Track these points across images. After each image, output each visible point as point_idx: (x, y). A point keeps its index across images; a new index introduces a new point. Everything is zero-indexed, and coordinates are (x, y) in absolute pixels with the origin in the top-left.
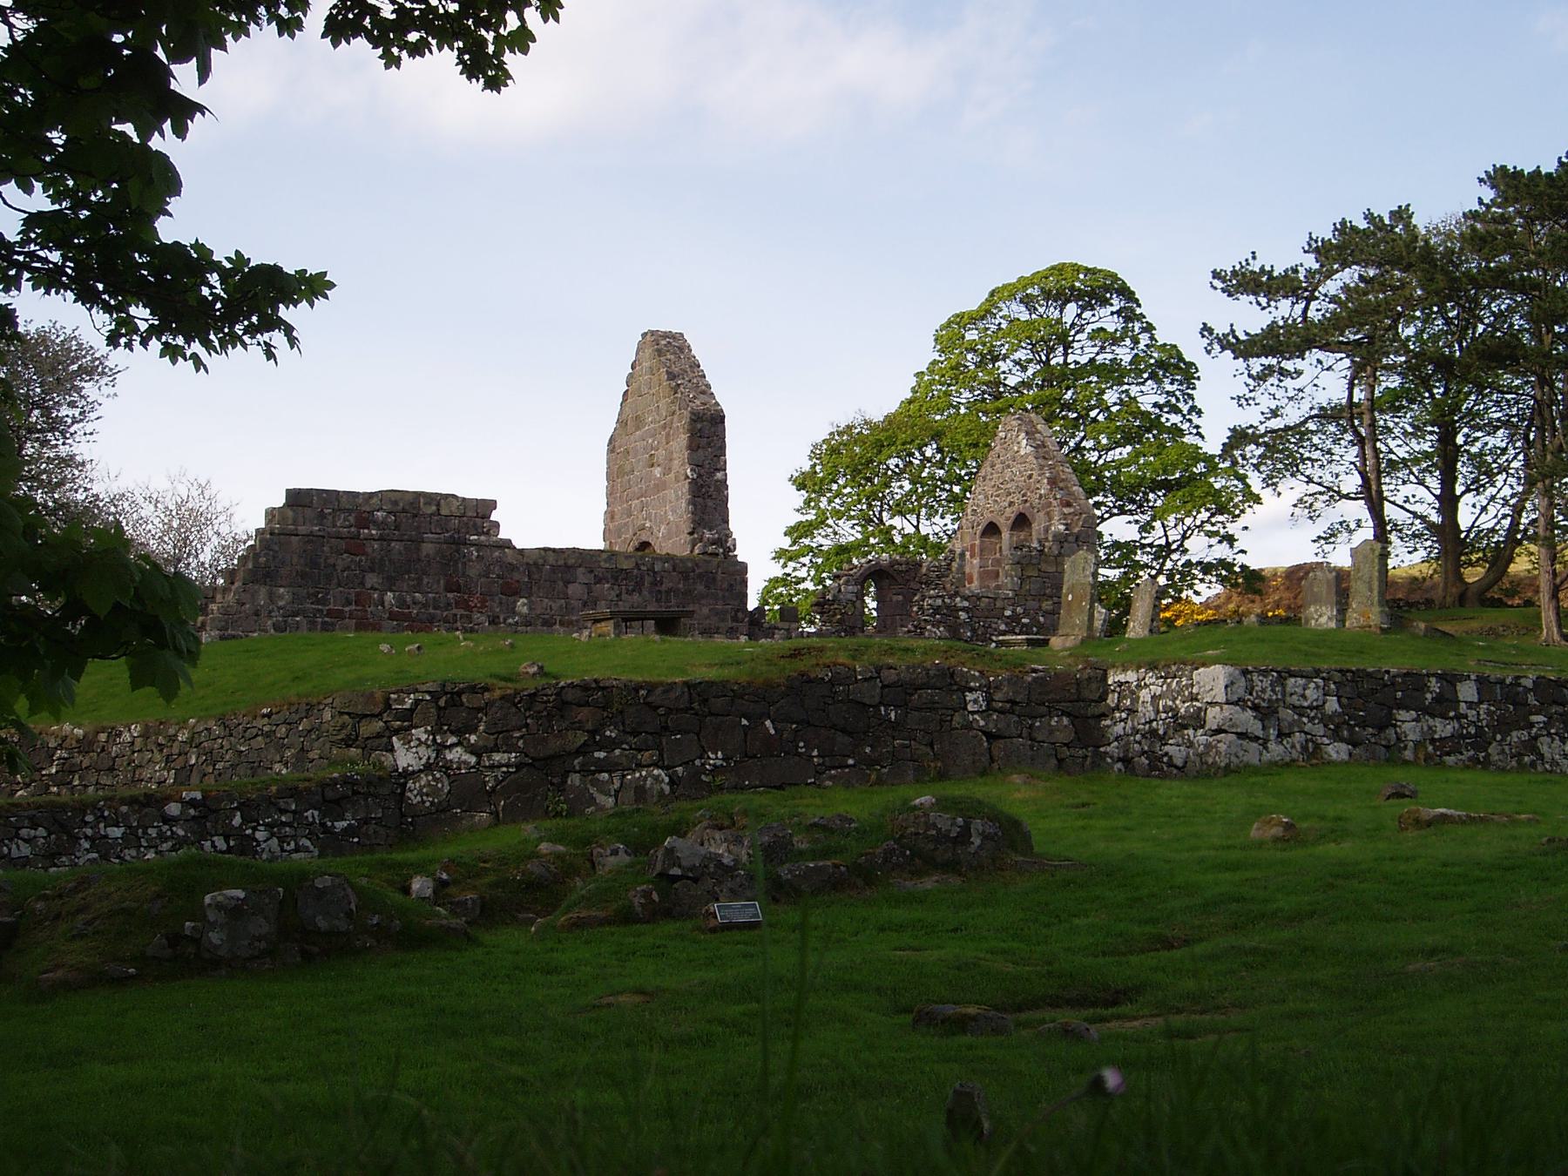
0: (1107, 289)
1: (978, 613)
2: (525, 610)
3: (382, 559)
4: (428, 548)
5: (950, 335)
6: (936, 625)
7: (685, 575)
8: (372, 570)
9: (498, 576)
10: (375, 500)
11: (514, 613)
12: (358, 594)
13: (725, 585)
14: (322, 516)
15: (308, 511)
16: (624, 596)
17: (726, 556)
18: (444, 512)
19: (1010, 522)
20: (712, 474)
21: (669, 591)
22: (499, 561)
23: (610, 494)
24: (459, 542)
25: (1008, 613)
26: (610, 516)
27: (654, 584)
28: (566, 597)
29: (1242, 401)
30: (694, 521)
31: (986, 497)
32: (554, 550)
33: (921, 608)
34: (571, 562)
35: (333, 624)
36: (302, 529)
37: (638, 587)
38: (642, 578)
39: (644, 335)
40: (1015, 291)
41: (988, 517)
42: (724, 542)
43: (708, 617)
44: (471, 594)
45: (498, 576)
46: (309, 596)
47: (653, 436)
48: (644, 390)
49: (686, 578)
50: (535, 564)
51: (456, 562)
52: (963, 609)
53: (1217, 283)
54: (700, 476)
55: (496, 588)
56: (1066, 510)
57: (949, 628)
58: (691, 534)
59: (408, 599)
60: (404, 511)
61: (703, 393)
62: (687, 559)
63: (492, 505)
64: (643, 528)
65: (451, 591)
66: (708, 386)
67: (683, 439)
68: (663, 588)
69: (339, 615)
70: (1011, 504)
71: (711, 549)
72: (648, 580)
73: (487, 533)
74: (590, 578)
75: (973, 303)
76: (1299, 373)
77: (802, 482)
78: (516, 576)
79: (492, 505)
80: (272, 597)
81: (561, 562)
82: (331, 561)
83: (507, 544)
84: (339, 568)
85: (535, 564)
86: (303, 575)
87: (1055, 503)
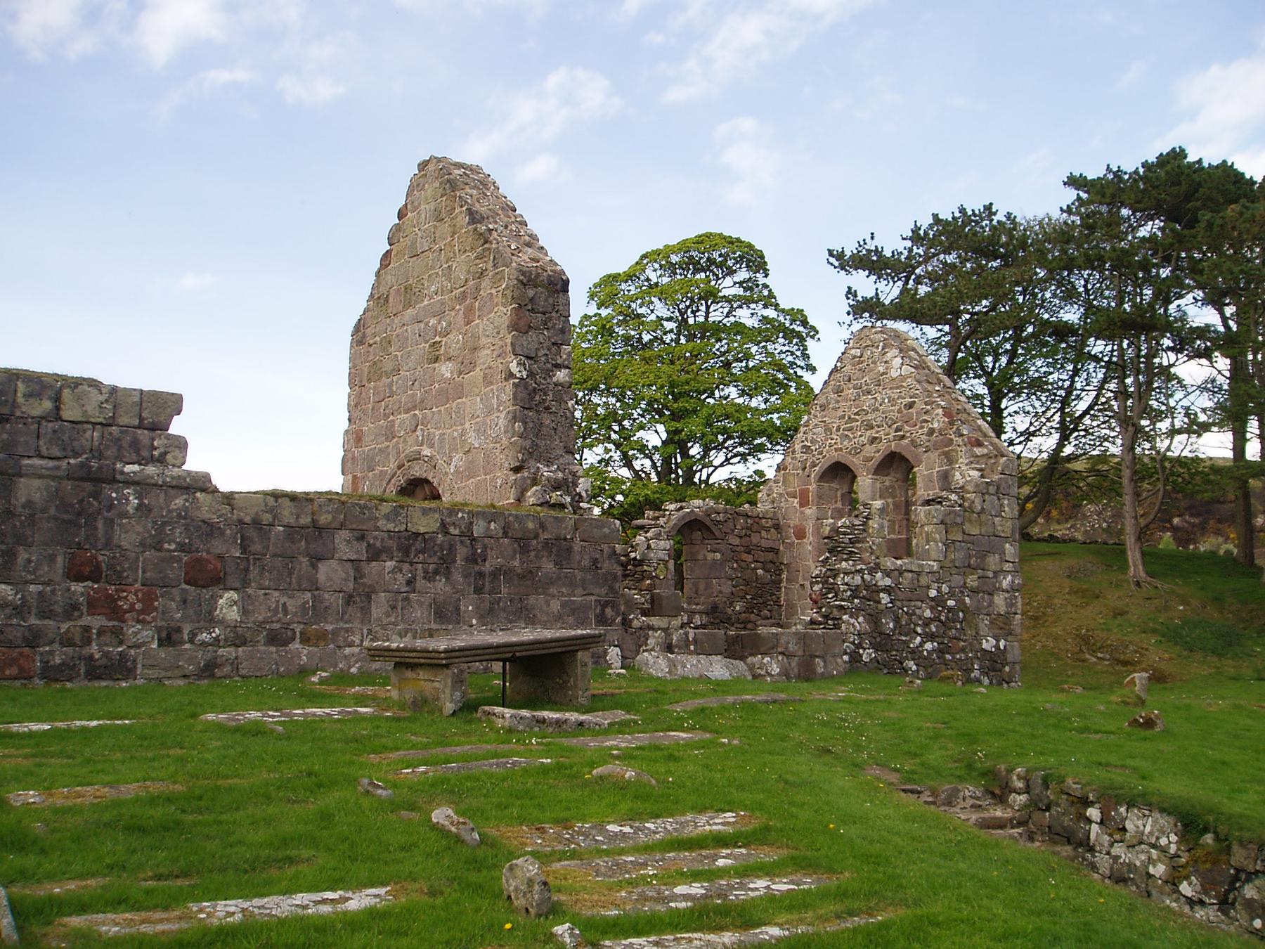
1: (901, 595)
2: (233, 614)
7: (523, 543)
9: (182, 547)
13: (586, 562)
16: (420, 583)
18: (69, 413)
19: (872, 464)
21: (495, 574)
23: (356, 405)
24: (98, 478)
25: (933, 593)
26: (354, 437)
27: (472, 559)
28: (314, 587)
30: (523, 449)
31: (828, 430)
32: (293, 497)
34: (324, 519)
37: (444, 567)
38: (452, 548)
39: (423, 165)
41: (831, 456)
45: (182, 547)
47: (440, 314)
48: (423, 244)
49: (525, 550)
50: (256, 522)
51: (91, 520)
52: (887, 590)
53: (832, 260)
54: (531, 374)
55: (175, 572)
58: (516, 470)
61: (529, 245)
63: (173, 404)
64: (416, 458)
65: (79, 578)
66: (534, 237)
67: (502, 314)
68: (488, 567)
70: (873, 440)
71: (555, 496)
72: (462, 552)
73: (161, 460)
74: (356, 551)
75: (622, 267)
78: (218, 546)
79: (173, 404)
81: (305, 520)
83: (201, 484)
85: (256, 522)
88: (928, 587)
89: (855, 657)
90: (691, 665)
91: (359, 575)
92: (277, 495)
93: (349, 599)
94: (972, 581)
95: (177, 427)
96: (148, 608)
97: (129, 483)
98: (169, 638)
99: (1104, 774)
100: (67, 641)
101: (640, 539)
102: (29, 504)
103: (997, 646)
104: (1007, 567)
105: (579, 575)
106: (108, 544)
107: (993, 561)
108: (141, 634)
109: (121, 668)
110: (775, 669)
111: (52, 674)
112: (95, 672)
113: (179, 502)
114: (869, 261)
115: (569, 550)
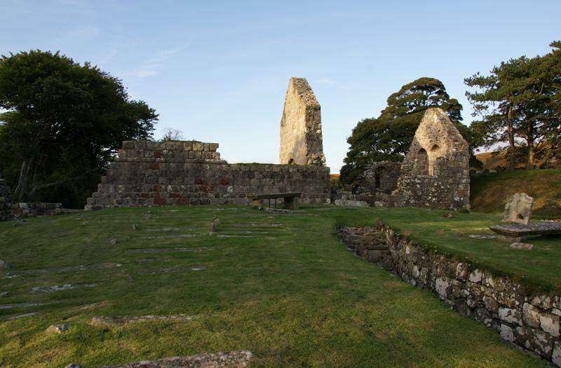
0: (435, 85)
3: (166, 171)
4: (187, 166)
5: (391, 100)
6: (408, 190)
8: (161, 175)
10: (162, 145)
11: (226, 192)
12: (155, 187)
14: (139, 153)
15: (132, 151)
17: (321, 165)
20: (316, 130)
22: (220, 170)
24: (201, 162)
25: (436, 184)
27: (289, 178)
29: (474, 114)
33: (401, 183)
35: (144, 200)
36: (129, 159)
40: (409, 87)
42: (320, 161)
43: (313, 191)
44: (207, 184)
45: (219, 177)
46: (133, 188)
51: (200, 171)
52: (418, 183)
55: (218, 182)
56: (456, 143)
57: (413, 191)
59: (178, 188)
60: (176, 149)
62: (306, 166)
63: (217, 146)
65: (198, 184)
67: (303, 117)
68: (293, 180)
69: (146, 196)
75: (397, 91)
76: (486, 108)
77: (350, 141)
78: (227, 176)
79: (217, 146)
80: (115, 189)
81: (247, 170)
82: (143, 172)
83: (225, 163)
84: (147, 176)
85: (236, 171)
86: (130, 179)
87: (451, 140)
88: (434, 183)
89: (408, 202)
90: (350, 203)
91: (260, 182)
92: (240, 164)
93: (258, 187)
94: (450, 181)
95: (218, 151)
96: (212, 190)
97: (207, 163)
98: (217, 196)
99: (464, 229)
100: (195, 197)
101: (365, 172)
102: (187, 168)
103: (460, 200)
104: (464, 177)
105: (318, 181)
106: (204, 177)
107: (459, 175)
108: (211, 195)
109: (207, 203)
110: (381, 205)
111: (194, 204)
112: (202, 203)
113: (218, 167)
114: (480, 82)
115: (316, 175)
